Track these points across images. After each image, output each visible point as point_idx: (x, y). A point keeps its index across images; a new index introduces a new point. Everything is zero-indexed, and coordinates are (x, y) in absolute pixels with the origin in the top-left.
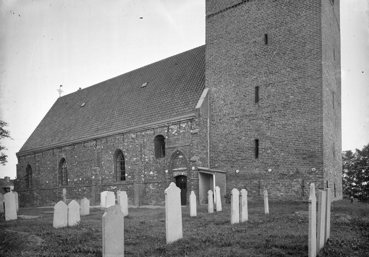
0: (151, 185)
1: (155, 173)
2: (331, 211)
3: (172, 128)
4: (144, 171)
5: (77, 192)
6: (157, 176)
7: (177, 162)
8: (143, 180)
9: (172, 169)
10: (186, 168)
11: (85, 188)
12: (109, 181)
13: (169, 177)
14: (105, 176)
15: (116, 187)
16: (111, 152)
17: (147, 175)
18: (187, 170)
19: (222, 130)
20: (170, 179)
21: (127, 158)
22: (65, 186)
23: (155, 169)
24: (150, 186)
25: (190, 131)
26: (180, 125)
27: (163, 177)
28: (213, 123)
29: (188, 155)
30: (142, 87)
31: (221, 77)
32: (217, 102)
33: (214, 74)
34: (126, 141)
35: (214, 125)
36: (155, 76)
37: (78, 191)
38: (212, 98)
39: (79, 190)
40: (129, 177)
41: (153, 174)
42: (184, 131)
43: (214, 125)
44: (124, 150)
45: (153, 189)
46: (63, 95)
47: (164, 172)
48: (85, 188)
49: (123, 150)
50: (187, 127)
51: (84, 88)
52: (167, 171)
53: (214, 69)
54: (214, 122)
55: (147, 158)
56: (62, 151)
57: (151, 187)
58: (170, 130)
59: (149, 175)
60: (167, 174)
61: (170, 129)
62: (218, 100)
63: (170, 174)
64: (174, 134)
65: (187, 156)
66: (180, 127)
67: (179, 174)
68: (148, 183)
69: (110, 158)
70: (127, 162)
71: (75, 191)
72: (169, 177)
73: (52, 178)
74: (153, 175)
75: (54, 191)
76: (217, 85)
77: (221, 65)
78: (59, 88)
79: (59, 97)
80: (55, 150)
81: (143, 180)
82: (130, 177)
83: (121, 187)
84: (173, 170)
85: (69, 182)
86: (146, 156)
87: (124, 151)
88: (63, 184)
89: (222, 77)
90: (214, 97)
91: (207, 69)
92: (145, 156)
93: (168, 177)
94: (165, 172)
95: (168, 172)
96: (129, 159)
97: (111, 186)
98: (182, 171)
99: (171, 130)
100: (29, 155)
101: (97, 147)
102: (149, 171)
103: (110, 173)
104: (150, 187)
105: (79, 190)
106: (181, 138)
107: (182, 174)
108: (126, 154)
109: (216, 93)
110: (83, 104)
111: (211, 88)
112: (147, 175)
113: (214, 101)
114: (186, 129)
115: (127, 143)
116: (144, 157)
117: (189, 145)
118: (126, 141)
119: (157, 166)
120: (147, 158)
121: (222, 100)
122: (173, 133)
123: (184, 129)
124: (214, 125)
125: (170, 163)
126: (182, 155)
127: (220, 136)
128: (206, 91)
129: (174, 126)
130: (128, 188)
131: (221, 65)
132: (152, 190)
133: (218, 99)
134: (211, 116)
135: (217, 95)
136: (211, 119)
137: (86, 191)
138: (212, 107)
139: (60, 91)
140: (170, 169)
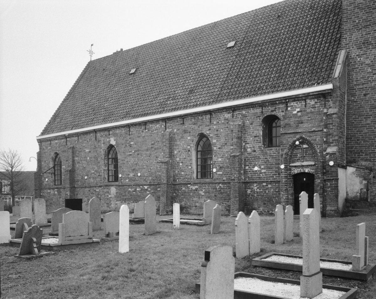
0: (255, 185)
1: (262, 169)
2: (130, 221)
3: (292, 106)
4: (244, 166)
5: (134, 193)
6: (264, 173)
7: (298, 153)
8: (243, 178)
9: (290, 164)
10: (313, 163)
11: (146, 187)
12: (186, 178)
13: (286, 174)
14: (178, 171)
15: (196, 187)
16: (189, 138)
17: (249, 172)
18: (315, 165)
19: (368, 110)
20: (287, 177)
21: (216, 147)
22: (113, 183)
23: (262, 163)
24: (254, 186)
25: (323, 111)
26: (306, 102)
27: (276, 175)
28: (354, 100)
29: (319, 144)
30: (228, 48)
31: (369, 34)
32: (360, 70)
33: (357, 30)
34: (215, 123)
35: (355, 102)
36: (196, 37)
37: (135, 191)
38: (353, 63)
39: (137, 189)
40: (219, 173)
41: (259, 169)
42: (313, 110)
43: (355, 103)
44: (211, 135)
45: (258, 190)
46: (94, 58)
47: (277, 168)
48: (146, 187)
49: (209, 136)
50: (318, 105)
51: (126, 50)
52: (282, 167)
53: (357, 22)
54: (355, 98)
55: (250, 148)
56: (109, 135)
57: (256, 188)
58: (289, 109)
59: (253, 171)
60: (283, 171)
61: (289, 106)
62: (362, 67)
63: (286, 170)
64: (296, 114)
65: (317, 147)
66: (306, 104)
67: (301, 170)
68: (251, 182)
69: (189, 146)
70: (215, 152)
71: (130, 191)
72: (286, 174)
73: (93, 172)
74: (259, 171)
75: (97, 190)
76: (362, 46)
77: (368, 17)
78: (89, 48)
79: (90, 60)
80: (98, 135)
81: (243, 178)
82: (221, 173)
83: (206, 187)
84: (291, 165)
85: (120, 178)
86: (248, 145)
87: (211, 137)
88: (110, 180)
89: (370, 33)
90: (355, 62)
91: (345, 22)
92: (245, 144)
93: (285, 174)
94: (279, 168)
95: (285, 167)
96: (219, 148)
97: (189, 185)
98: (307, 166)
99: (291, 108)
100: (57, 140)
101: (167, 130)
102: (253, 165)
103: (188, 167)
104: (253, 188)
105: (137, 189)
106: (307, 120)
107: (307, 171)
108: (214, 141)
109: (359, 57)
110: (133, 71)
111: (352, 50)
112: (249, 172)
113: (355, 68)
114: (316, 107)
115: (216, 125)
116: (244, 146)
117: (321, 131)
118: (215, 123)
119: (267, 158)
120: (250, 148)
121: (370, 66)
122: (295, 112)
123: (312, 108)
124: (355, 102)
125: (288, 154)
126: (307, 144)
127: (364, 118)
128: (342, 55)
129: (296, 103)
130: (216, 188)
131: (368, 17)
132: (257, 192)
133: (362, 65)
134: (350, 90)
135: (360, 59)
136: (350, 94)
137: (149, 191)
138: (352, 77)
139: (91, 52)
140: (287, 164)
